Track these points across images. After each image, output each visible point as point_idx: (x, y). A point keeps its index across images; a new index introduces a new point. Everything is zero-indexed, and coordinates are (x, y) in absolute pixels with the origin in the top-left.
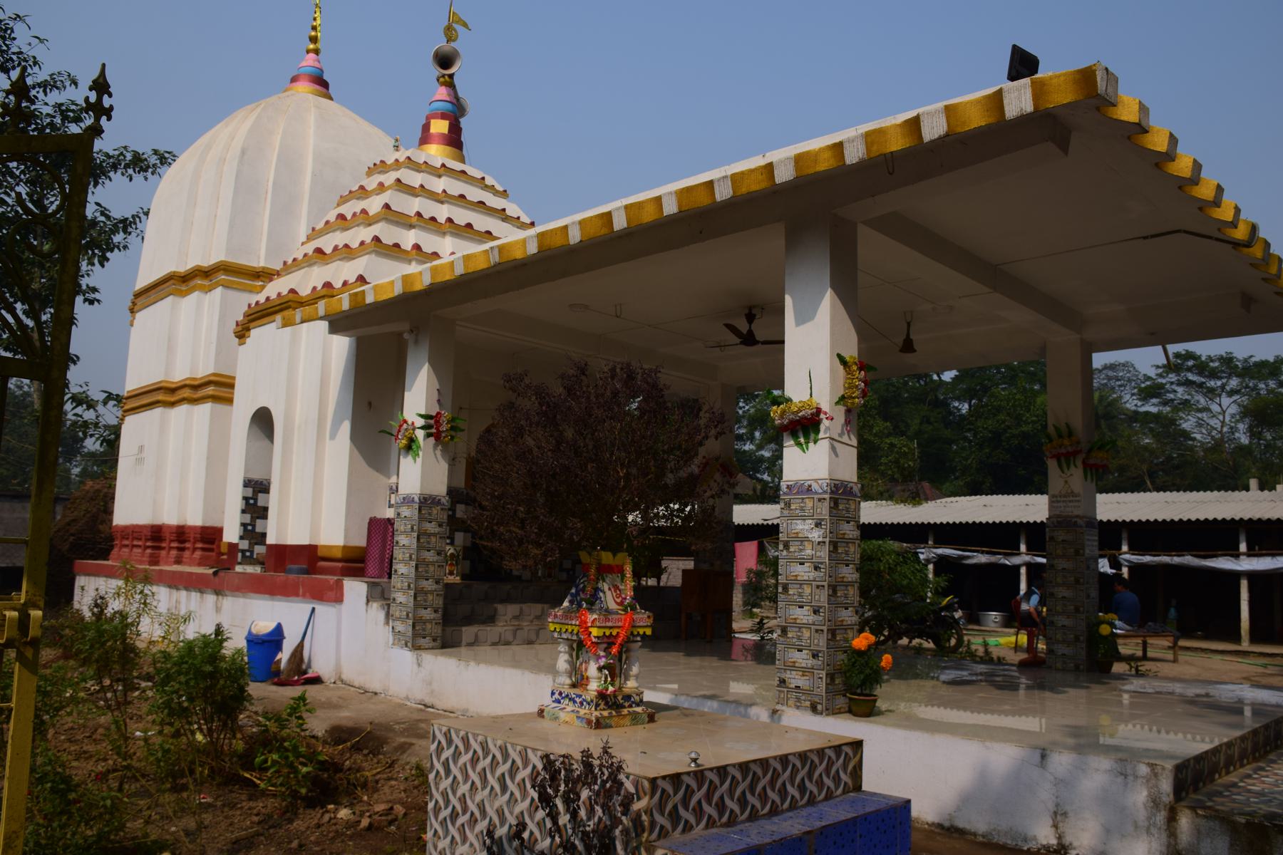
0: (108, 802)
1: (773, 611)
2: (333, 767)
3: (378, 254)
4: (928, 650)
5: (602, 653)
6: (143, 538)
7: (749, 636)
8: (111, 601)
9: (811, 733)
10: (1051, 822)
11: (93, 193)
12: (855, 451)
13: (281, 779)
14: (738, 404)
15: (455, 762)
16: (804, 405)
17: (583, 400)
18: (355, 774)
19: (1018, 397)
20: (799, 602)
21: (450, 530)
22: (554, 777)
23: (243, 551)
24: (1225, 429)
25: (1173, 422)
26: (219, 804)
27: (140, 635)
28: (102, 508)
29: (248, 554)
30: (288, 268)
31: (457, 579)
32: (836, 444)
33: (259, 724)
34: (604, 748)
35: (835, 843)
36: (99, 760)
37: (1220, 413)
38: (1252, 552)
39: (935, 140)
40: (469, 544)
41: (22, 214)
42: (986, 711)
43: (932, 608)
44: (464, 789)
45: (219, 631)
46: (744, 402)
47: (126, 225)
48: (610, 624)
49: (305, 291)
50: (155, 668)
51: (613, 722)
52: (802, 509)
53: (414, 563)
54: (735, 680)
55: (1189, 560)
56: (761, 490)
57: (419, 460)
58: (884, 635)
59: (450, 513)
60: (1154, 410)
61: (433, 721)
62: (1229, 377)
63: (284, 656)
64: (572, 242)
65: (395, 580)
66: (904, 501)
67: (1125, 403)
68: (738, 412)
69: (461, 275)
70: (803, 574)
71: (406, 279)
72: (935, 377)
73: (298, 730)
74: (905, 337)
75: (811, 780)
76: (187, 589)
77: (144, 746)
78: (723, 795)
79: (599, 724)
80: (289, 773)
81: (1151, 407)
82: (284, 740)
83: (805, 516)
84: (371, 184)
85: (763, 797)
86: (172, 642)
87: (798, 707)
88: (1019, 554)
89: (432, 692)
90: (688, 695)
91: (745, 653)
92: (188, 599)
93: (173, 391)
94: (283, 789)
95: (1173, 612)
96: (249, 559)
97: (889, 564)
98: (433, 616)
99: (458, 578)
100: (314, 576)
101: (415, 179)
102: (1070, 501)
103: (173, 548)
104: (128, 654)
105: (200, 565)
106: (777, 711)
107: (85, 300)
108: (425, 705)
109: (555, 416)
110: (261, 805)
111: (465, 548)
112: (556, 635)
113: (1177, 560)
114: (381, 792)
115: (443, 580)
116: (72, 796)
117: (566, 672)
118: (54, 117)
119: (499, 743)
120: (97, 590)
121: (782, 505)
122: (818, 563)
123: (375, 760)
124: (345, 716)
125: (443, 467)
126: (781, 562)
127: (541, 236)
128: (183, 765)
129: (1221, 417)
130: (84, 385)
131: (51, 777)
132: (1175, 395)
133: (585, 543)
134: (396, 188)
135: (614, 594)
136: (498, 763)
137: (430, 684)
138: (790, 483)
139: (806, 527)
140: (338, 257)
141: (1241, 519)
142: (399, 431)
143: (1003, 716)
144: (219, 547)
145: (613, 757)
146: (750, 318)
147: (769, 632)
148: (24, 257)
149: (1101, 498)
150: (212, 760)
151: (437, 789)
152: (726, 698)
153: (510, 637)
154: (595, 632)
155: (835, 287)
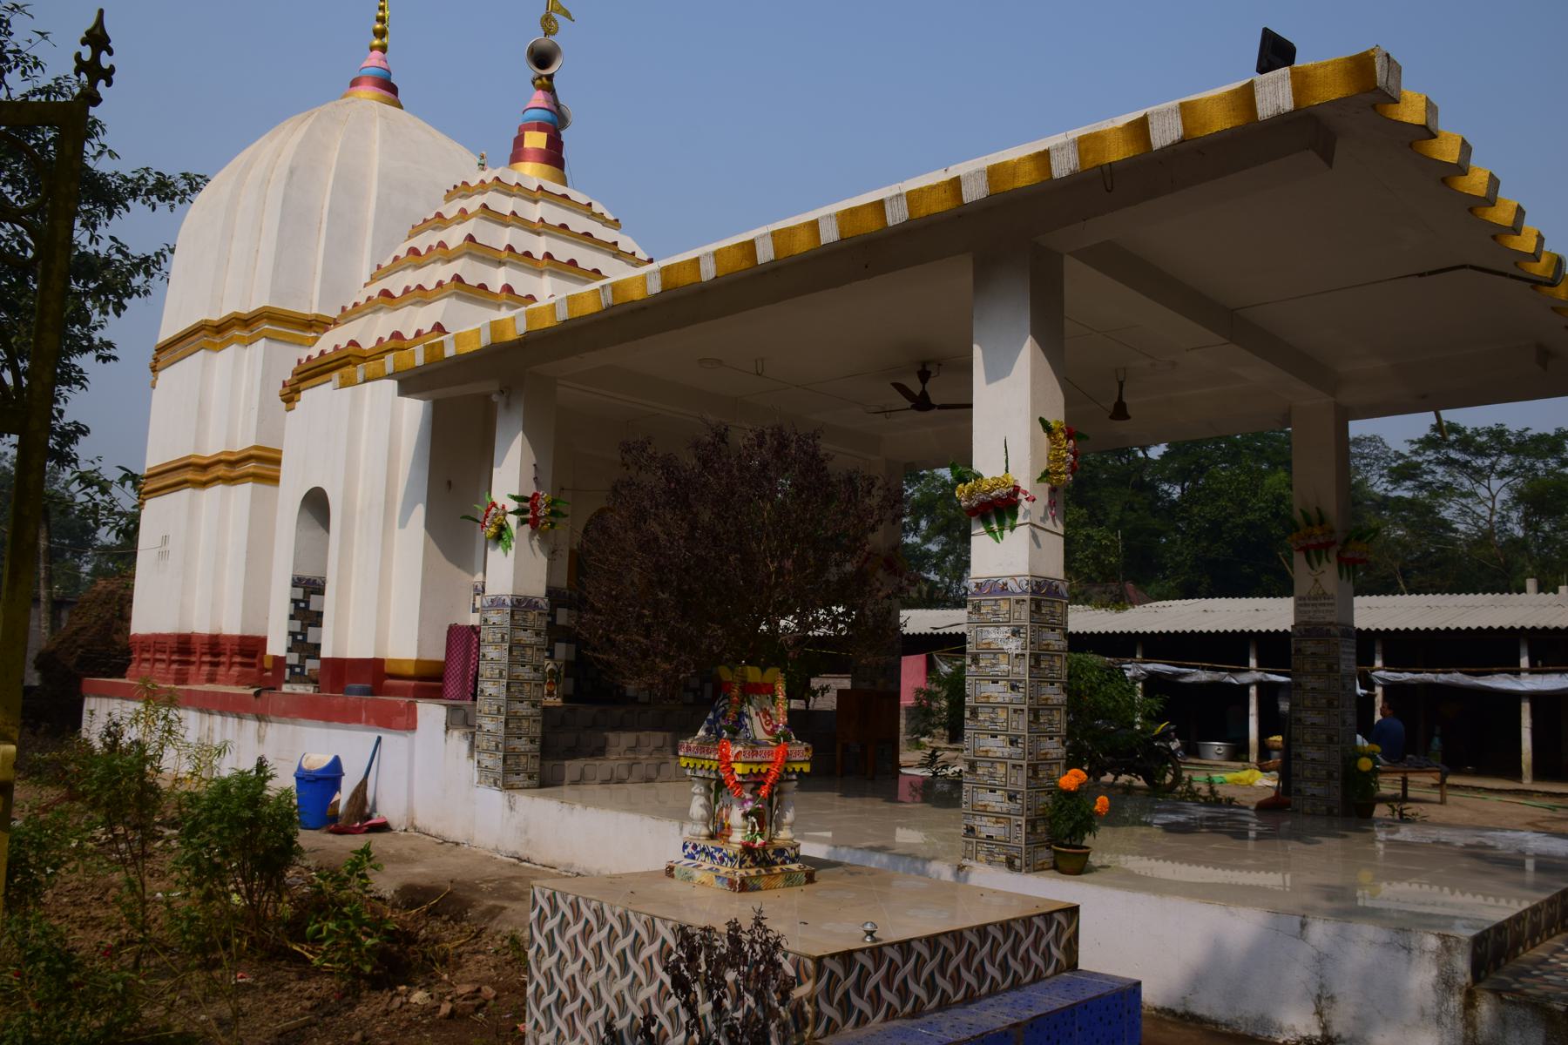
0: (120, 986)
2: (405, 937)
3: (459, 296)
5: (748, 796)
6: (168, 650)
7: (918, 772)
8: (127, 729)
9: (1009, 896)
10: (1313, 1009)
11: (107, 225)
12: (1061, 540)
13: (340, 953)
15: (562, 935)
16: (998, 483)
17: (723, 474)
19: (1242, 478)
20: (992, 730)
21: (550, 640)
22: (692, 958)
23: (292, 667)
24: (1495, 518)
25: (1430, 509)
26: (261, 984)
27: (161, 772)
28: (117, 614)
29: (298, 670)
30: (347, 315)
31: (558, 702)
33: (311, 882)
35: (1048, 1038)
36: (110, 928)
37: (1489, 499)
38: (1535, 669)
39: (1167, 146)
40: (572, 657)
41: (19, 251)
42: (1224, 867)
44: (573, 968)
45: (261, 765)
47: (148, 265)
48: (758, 759)
49: (368, 344)
50: (181, 813)
51: (761, 883)
52: (995, 614)
54: (902, 826)
55: (1458, 678)
56: (928, 592)
57: (511, 553)
59: (550, 619)
60: (1408, 495)
61: (533, 882)
62: (1500, 455)
63: (343, 797)
64: (704, 279)
65: (481, 703)
66: (1104, 606)
67: (1372, 486)
70: (996, 694)
71: (495, 326)
72: (1140, 454)
73: (361, 891)
74: (1116, 400)
75: (1015, 957)
76: (222, 713)
78: (906, 977)
79: (744, 886)
80: (350, 946)
81: (1404, 491)
84: (451, 210)
85: (957, 980)
86: (204, 780)
87: (990, 863)
88: (1248, 671)
89: (528, 841)
90: (850, 846)
92: (223, 725)
93: (204, 467)
95: (1436, 741)
96: (299, 677)
98: (529, 747)
99: (559, 700)
101: (505, 205)
102: (1321, 605)
103: (235, 663)
104: (148, 795)
105: (237, 683)
106: (964, 867)
107: (98, 357)
108: (518, 858)
109: (688, 495)
110: (314, 985)
112: (689, 772)
113: (1442, 678)
115: (541, 702)
116: (73, 978)
117: (702, 820)
119: (618, 910)
120: (110, 714)
121: (970, 608)
124: (420, 873)
125: (542, 561)
127: (666, 271)
128: (215, 936)
129: (1490, 504)
130: (96, 461)
132: (1434, 477)
133: (728, 656)
134: (481, 215)
135: (763, 720)
136: (617, 936)
137: (526, 832)
138: (979, 581)
140: (410, 302)
141: (1523, 628)
142: (486, 517)
143: (1245, 872)
144: (262, 661)
145: (768, 931)
146: (924, 376)
147: (943, 767)
148: (22, 304)
149: (1360, 602)
150: (253, 930)
151: (539, 969)
153: (624, 774)
154: (739, 768)
155: (1036, 334)
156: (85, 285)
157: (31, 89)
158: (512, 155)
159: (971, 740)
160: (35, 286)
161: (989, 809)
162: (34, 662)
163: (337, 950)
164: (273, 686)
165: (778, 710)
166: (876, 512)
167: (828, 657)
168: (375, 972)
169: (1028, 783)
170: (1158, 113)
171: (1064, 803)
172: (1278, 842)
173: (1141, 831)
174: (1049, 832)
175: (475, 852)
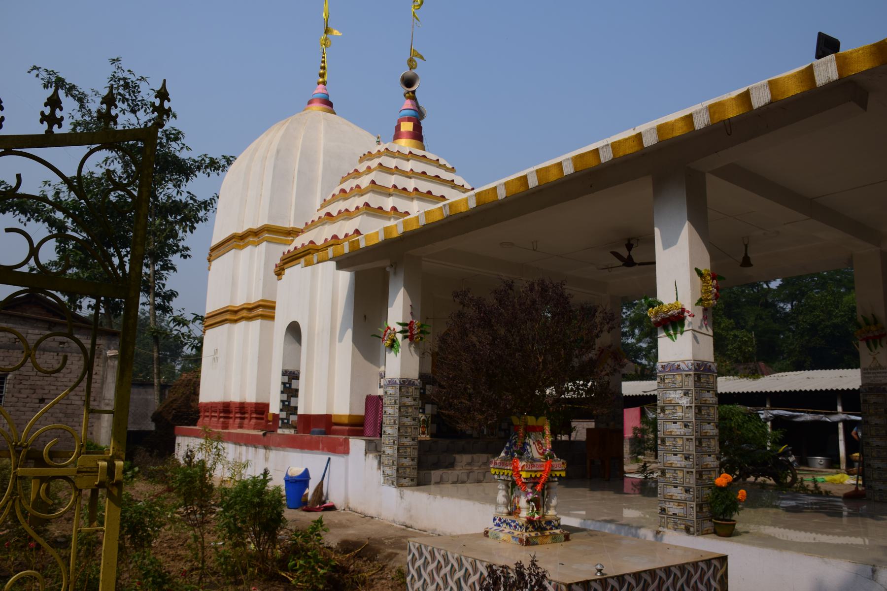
1: (653, 457)
2: (341, 569)
3: (368, 214)
4: (770, 485)
5: (530, 490)
7: (636, 476)
8: (196, 453)
9: (686, 550)
12: (711, 339)
13: (306, 577)
14: (622, 310)
15: (425, 569)
16: (672, 307)
18: (357, 574)
19: (828, 298)
20: (674, 451)
21: (422, 403)
23: (283, 419)
28: (193, 391)
29: (286, 421)
30: (309, 227)
31: (428, 437)
32: (698, 335)
34: (532, 561)
36: (187, 561)
39: (762, 107)
43: (772, 454)
46: (626, 309)
47: (206, 205)
48: (535, 469)
49: (320, 242)
51: (538, 540)
52: (674, 383)
53: (397, 427)
54: (625, 507)
56: (641, 371)
57: (399, 355)
58: (736, 475)
59: (422, 391)
63: (310, 491)
66: (746, 376)
68: (622, 317)
69: (424, 225)
71: (386, 230)
72: (765, 286)
74: (744, 255)
76: (246, 445)
77: (215, 553)
79: (528, 542)
80: (312, 573)
82: (308, 550)
83: (676, 388)
87: (675, 529)
88: (837, 413)
89: (411, 517)
90: (593, 520)
91: (634, 488)
92: (247, 452)
93: (236, 312)
94: (308, 585)
96: (286, 425)
97: (738, 422)
98: (411, 463)
99: (428, 436)
100: (329, 436)
101: (391, 163)
102: (878, 373)
103: (253, 418)
105: (254, 429)
106: (660, 532)
107: (182, 256)
108: (406, 526)
111: (433, 416)
114: (375, 588)
118: (162, 139)
119: (456, 556)
121: (659, 380)
122: (688, 422)
123: (371, 565)
124: (351, 533)
125: (416, 359)
126: (659, 422)
127: (478, 195)
130: (182, 310)
131: (152, 574)
135: (538, 447)
136: (456, 570)
137: (410, 511)
139: (677, 396)
142: (385, 335)
144: (267, 416)
145: (538, 568)
146: (629, 247)
147: (651, 473)
150: (260, 564)
152: (620, 522)
153: (465, 478)
155: (688, 220)
156: (175, 217)
157: (149, 118)
158: (394, 136)
159: (662, 457)
160: (151, 220)
161: (674, 498)
162: (151, 418)
163: (304, 576)
164: (272, 430)
165: (546, 441)
166: (599, 326)
167: (578, 409)
168: (326, 589)
169: (697, 482)
170: (755, 88)
171: (719, 494)
172: (859, 518)
173: (772, 511)
174: (710, 512)
175: (382, 522)
